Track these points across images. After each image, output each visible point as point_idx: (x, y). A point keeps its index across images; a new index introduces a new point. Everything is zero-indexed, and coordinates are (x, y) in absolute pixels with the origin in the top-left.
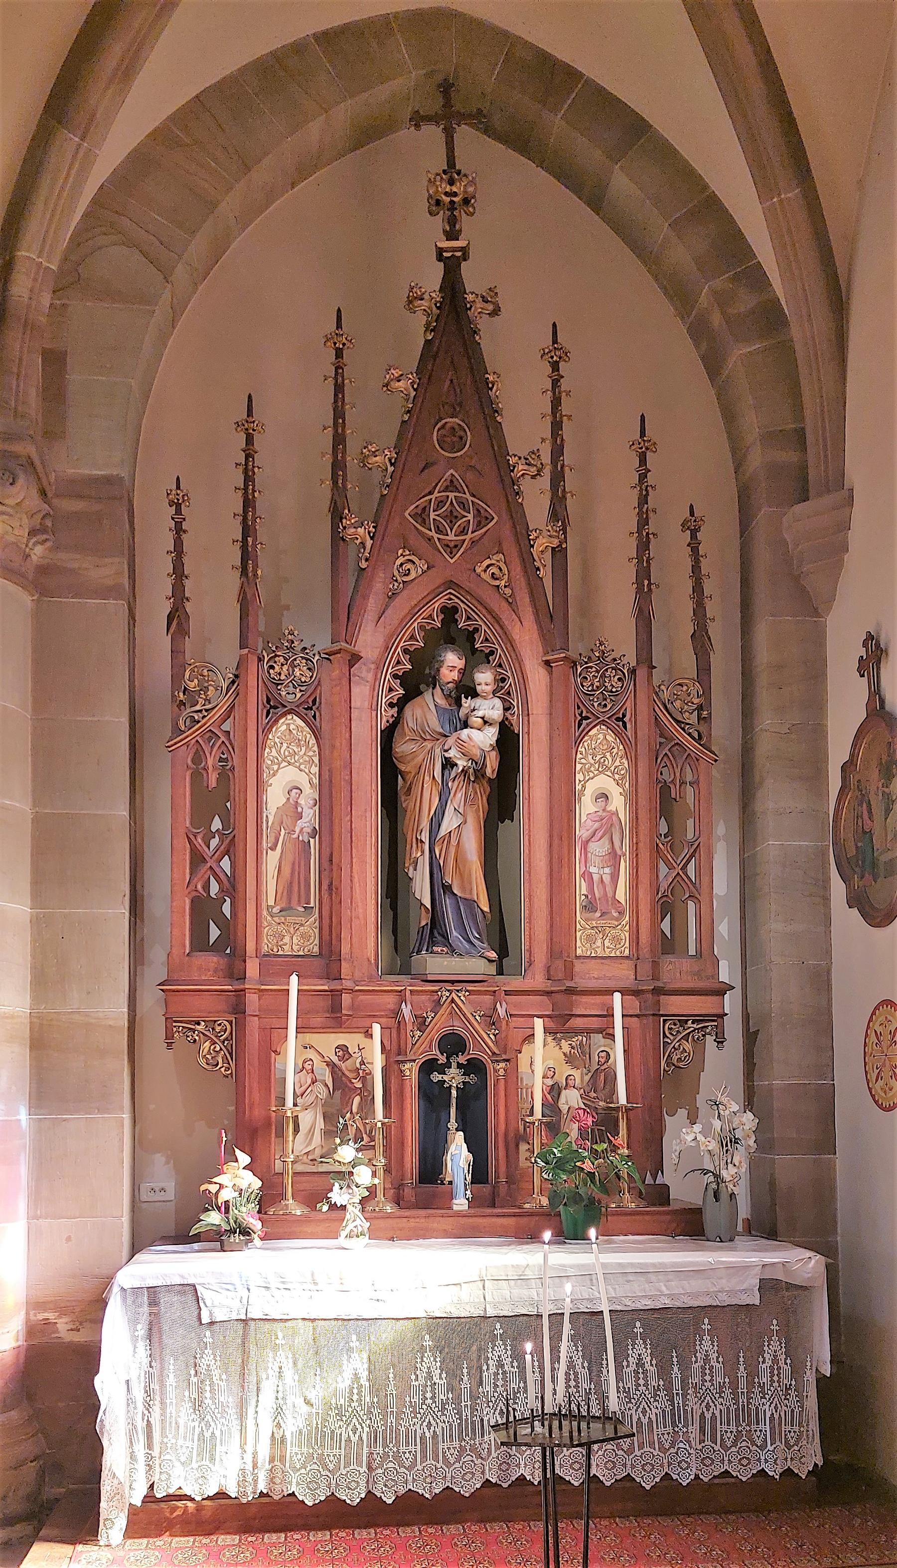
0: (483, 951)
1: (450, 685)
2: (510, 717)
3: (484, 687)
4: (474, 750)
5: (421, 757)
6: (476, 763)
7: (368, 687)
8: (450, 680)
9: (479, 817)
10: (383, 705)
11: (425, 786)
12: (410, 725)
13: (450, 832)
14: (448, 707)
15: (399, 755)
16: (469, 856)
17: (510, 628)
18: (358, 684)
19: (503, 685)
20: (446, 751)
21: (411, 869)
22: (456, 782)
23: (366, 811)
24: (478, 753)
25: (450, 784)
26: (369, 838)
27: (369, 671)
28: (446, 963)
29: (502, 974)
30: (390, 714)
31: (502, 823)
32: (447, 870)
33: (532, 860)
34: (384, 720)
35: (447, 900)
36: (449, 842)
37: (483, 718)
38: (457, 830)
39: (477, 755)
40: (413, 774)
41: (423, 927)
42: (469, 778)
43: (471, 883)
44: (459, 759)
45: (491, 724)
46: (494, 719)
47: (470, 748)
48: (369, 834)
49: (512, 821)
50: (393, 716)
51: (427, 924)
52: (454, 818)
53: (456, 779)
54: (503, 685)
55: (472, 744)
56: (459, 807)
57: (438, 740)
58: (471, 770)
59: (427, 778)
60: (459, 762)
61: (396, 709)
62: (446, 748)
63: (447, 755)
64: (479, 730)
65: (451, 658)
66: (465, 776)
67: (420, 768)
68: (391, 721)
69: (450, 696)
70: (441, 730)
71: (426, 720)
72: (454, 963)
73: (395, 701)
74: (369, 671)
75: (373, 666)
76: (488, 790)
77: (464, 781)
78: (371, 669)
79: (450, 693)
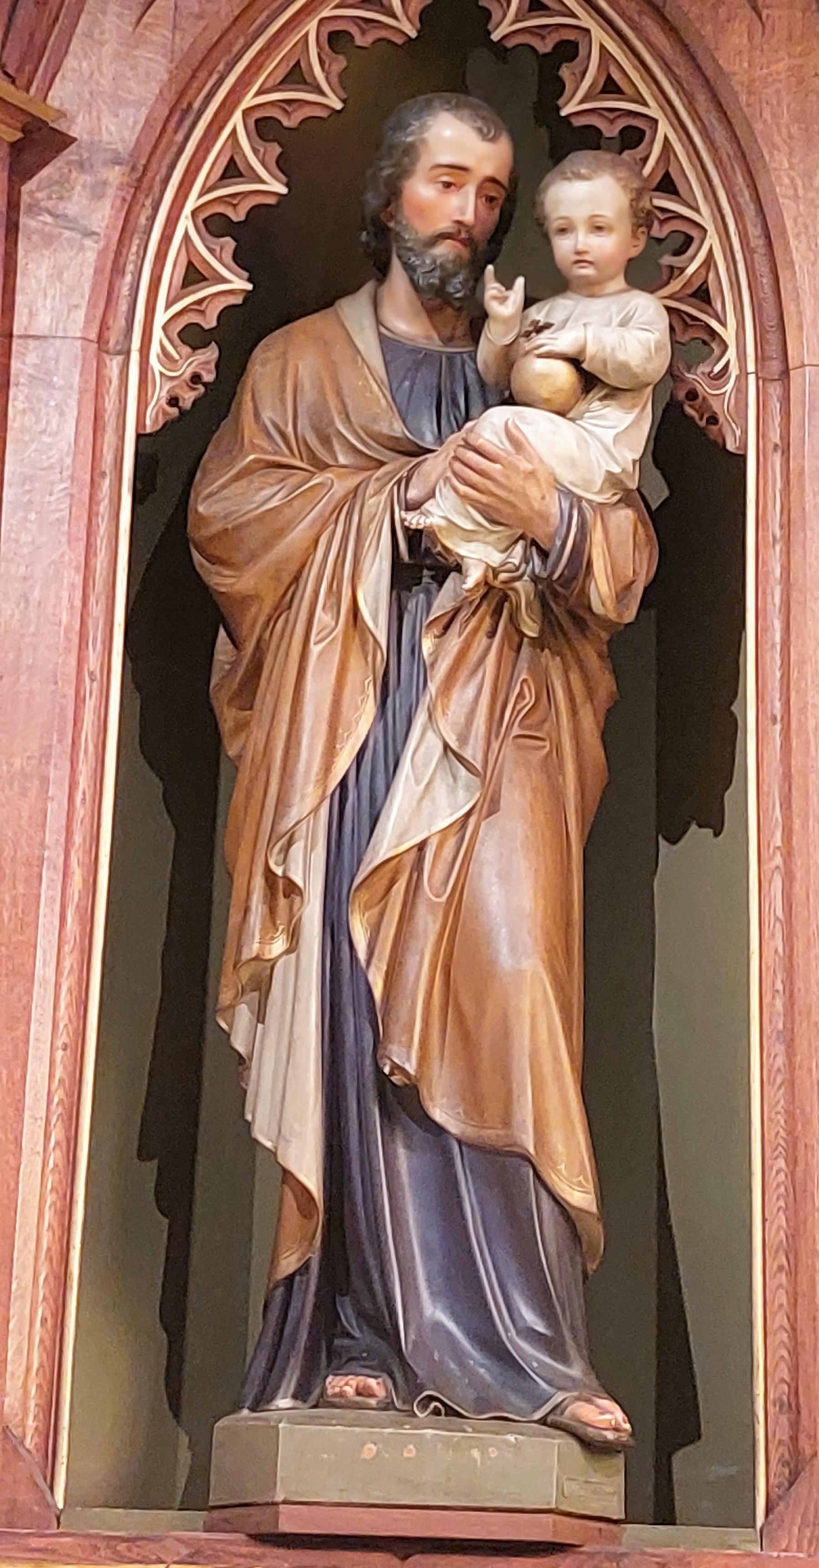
0: (559, 1397)
1: (444, 250)
2: (704, 388)
3: (584, 239)
4: (534, 492)
5: (300, 532)
6: (544, 554)
7: (91, 256)
8: (444, 225)
9: (556, 795)
10: (158, 333)
11: (315, 650)
12: (267, 415)
13: (421, 847)
14: (436, 345)
15: (206, 532)
16: (505, 958)
17: (708, 30)
18: (49, 240)
19: (676, 261)
20: (412, 507)
21: (244, 1014)
22: (454, 642)
23: (45, 756)
24: (554, 506)
25: (427, 645)
26: (50, 876)
27: (97, 192)
28: (370, 1450)
29: (670, 1520)
30: (186, 371)
31: (673, 841)
32: (402, 1011)
33: (799, 984)
34: (159, 394)
35: (402, 1153)
36: (413, 890)
37: (575, 361)
38: (451, 842)
39: (545, 517)
40: (267, 609)
41: (290, 1278)
42: (513, 619)
43: (505, 1073)
44: (468, 536)
45: (613, 393)
46: (624, 367)
47: (517, 482)
48: (54, 854)
49: (717, 834)
50: (196, 378)
51: (305, 1268)
52: (441, 789)
53: (456, 627)
54: (676, 261)
55: (525, 466)
56: (463, 739)
57: (382, 464)
58: (523, 587)
59: (322, 617)
60: (463, 549)
61: (211, 353)
62: (413, 493)
63: (415, 520)
64: (562, 414)
65: (448, 133)
66: (497, 613)
67: (296, 579)
68: (188, 398)
69: (440, 291)
70: (398, 429)
71: (339, 393)
72: (410, 1452)
73: (210, 322)
74: (97, 192)
75: (115, 175)
76: (606, 684)
77: (492, 634)
78: (105, 183)
79: (444, 281)
